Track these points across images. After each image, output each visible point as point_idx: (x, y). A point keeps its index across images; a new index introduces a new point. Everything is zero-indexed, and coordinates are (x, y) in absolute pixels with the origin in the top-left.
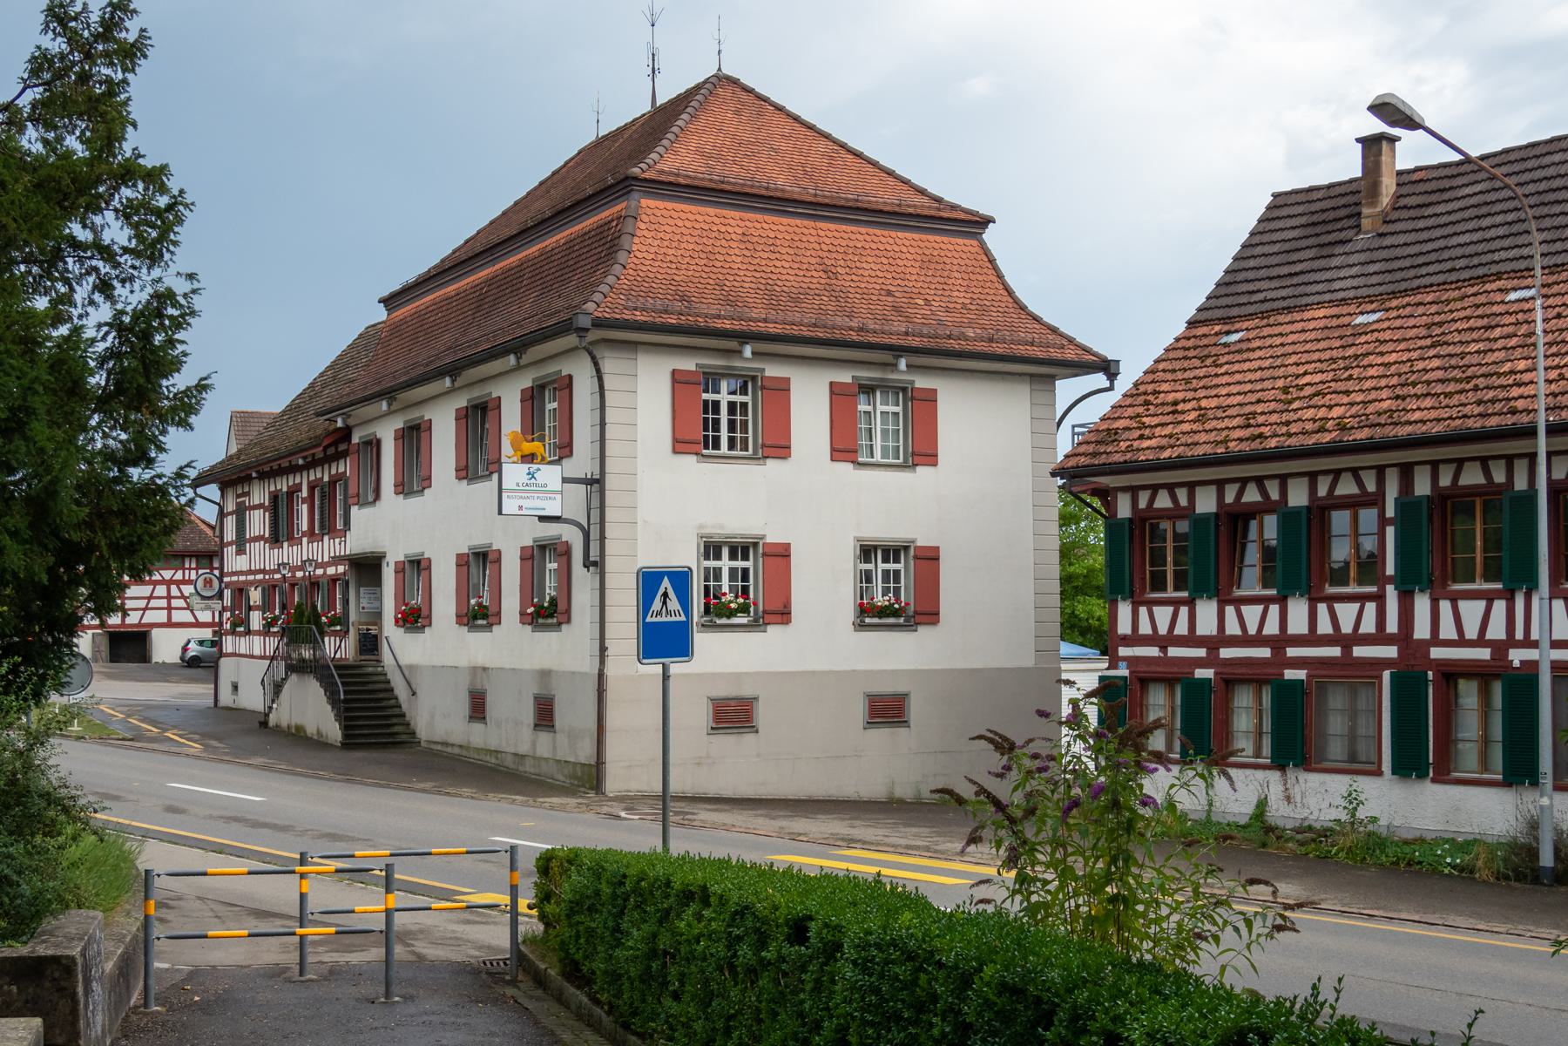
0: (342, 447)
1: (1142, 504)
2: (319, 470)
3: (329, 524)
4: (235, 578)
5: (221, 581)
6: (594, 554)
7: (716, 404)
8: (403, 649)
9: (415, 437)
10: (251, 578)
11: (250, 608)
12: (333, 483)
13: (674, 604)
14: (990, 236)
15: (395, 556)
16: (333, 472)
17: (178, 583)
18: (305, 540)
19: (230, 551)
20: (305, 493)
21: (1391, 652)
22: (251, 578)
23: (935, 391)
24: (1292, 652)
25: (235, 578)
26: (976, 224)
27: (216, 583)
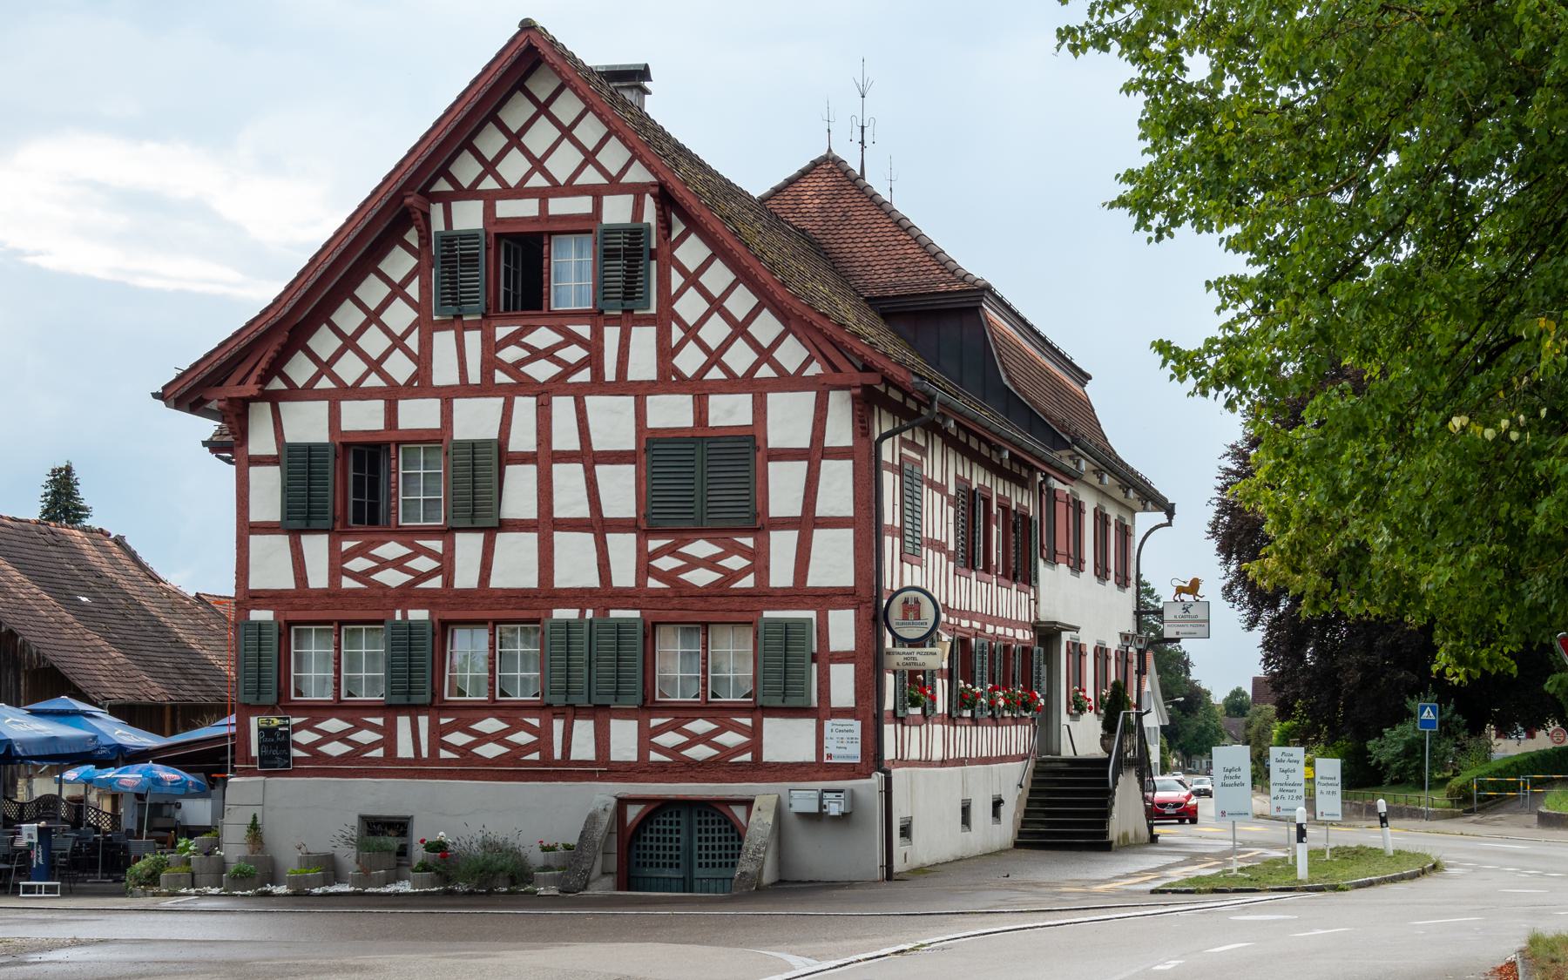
26: (1083, 377)
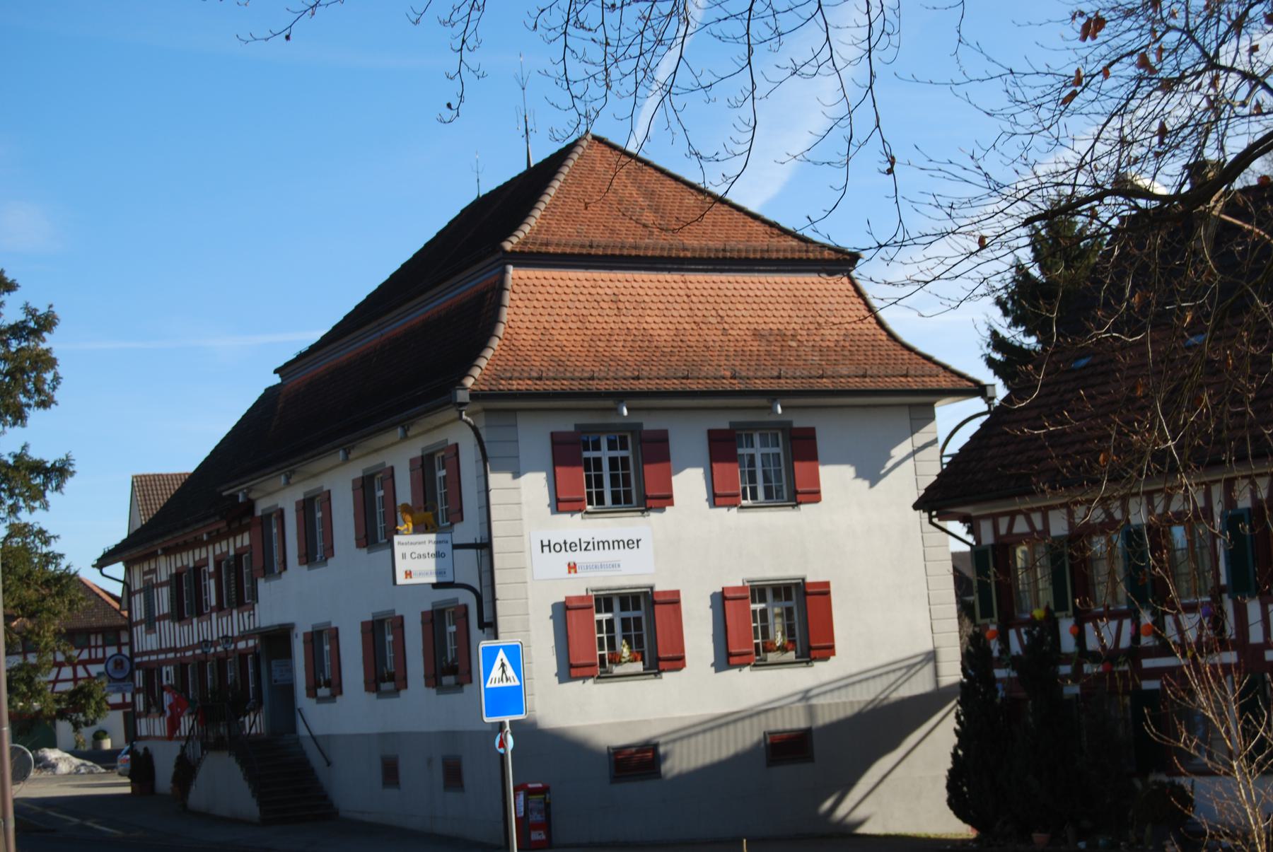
0: (246, 521)
1: (1003, 531)
2: (224, 543)
3: (239, 596)
4: (145, 658)
5: (131, 659)
6: (487, 617)
7: (598, 462)
8: (319, 718)
9: (313, 510)
10: (162, 657)
11: (163, 689)
12: (238, 556)
13: (510, 672)
14: (861, 271)
15: (303, 627)
16: (239, 545)
17: (84, 663)
18: (214, 615)
19: (139, 631)
20: (211, 568)
21: (1231, 657)
22: (162, 657)
23: (813, 430)
24: (1147, 663)
25: (145, 658)
27: (127, 664)
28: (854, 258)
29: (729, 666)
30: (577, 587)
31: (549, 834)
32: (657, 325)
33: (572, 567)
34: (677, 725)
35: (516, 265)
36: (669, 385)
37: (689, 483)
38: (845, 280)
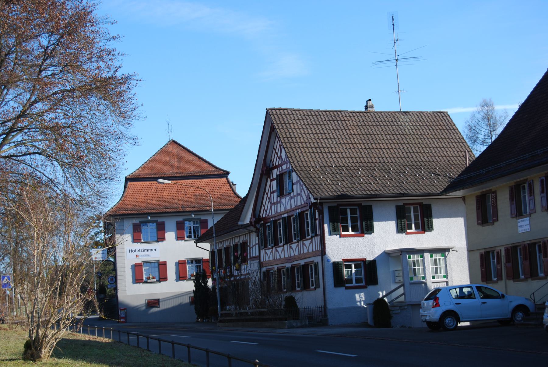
28: (228, 173)
29: (180, 280)
30: (138, 261)
31: (126, 320)
32: (167, 195)
33: (137, 256)
34: (174, 294)
35: (130, 181)
36: (161, 211)
37: (170, 235)
38: (225, 179)
